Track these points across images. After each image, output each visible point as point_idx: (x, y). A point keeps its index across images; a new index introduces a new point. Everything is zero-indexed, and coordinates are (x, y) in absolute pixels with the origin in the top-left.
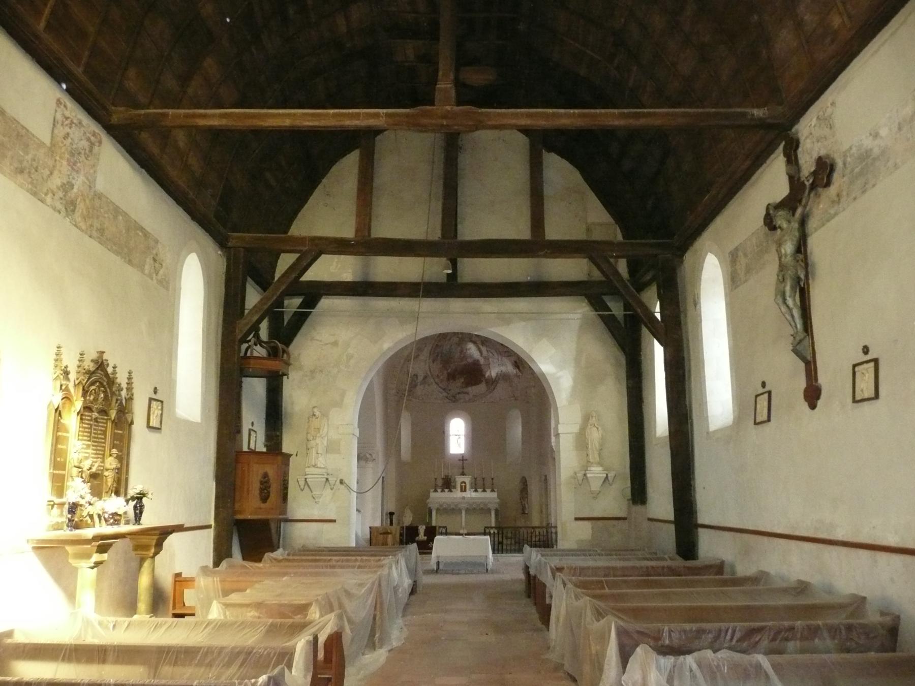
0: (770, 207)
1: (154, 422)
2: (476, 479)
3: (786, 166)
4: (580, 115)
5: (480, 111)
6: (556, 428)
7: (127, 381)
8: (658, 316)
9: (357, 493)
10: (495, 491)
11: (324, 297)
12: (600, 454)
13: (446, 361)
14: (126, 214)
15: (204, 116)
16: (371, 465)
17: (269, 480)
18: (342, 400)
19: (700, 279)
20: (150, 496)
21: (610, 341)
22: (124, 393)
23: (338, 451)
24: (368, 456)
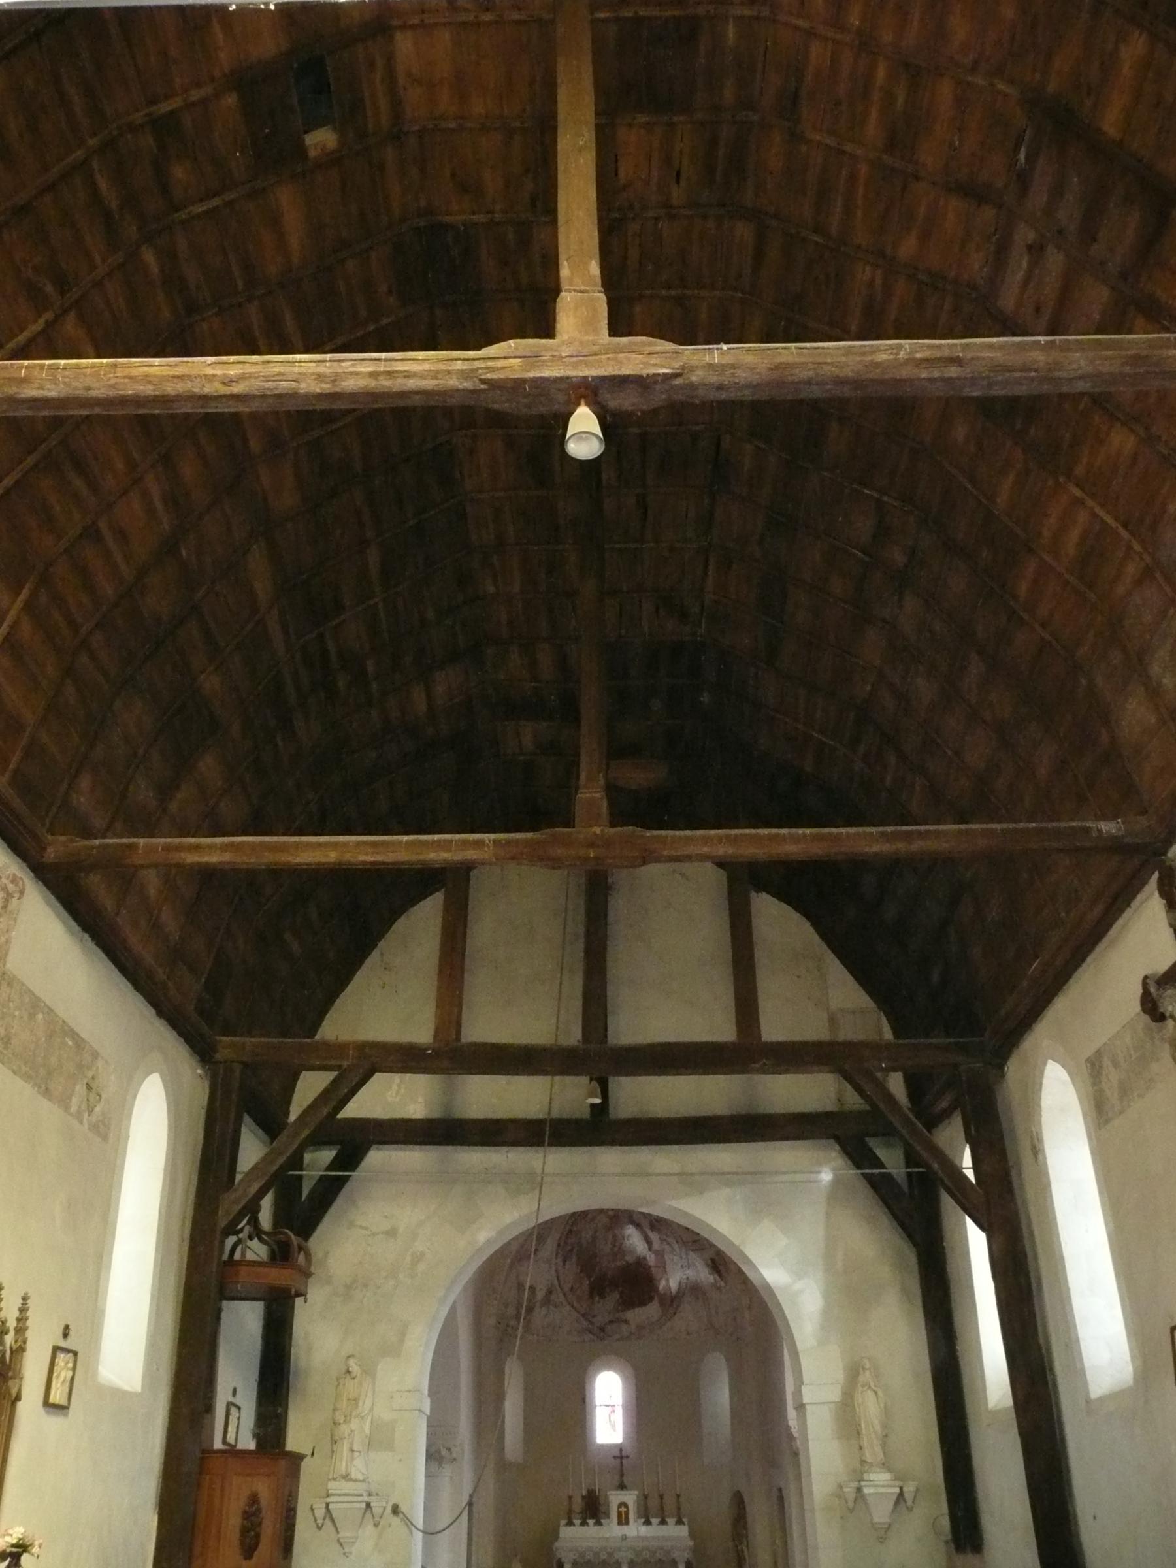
0: (1148, 981)
1: (57, 1396)
2: (646, 1497)
3: (1167, 912)
4: (815, 838)
5: (648, 834)
6: (798, 1393)
7: (17, 1314)
8: (970, 1174)
9: (424, 1532)
10: (684, 1524)
11: (375, 1146)
12: (884, 1445)
13: (587, 1261)
14: (51, 1010)
15: (197, 848)
16: (447, 1470)
17: (259, 1510)
18: (402, 1341)
19: (1039, 1106)
20: (35, 1550)
21: (885, 1220)
22: (9, 1339)
23: (389, 1446)
24: (444, 1452)
